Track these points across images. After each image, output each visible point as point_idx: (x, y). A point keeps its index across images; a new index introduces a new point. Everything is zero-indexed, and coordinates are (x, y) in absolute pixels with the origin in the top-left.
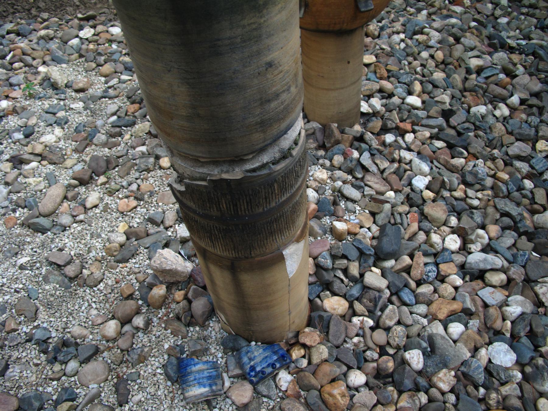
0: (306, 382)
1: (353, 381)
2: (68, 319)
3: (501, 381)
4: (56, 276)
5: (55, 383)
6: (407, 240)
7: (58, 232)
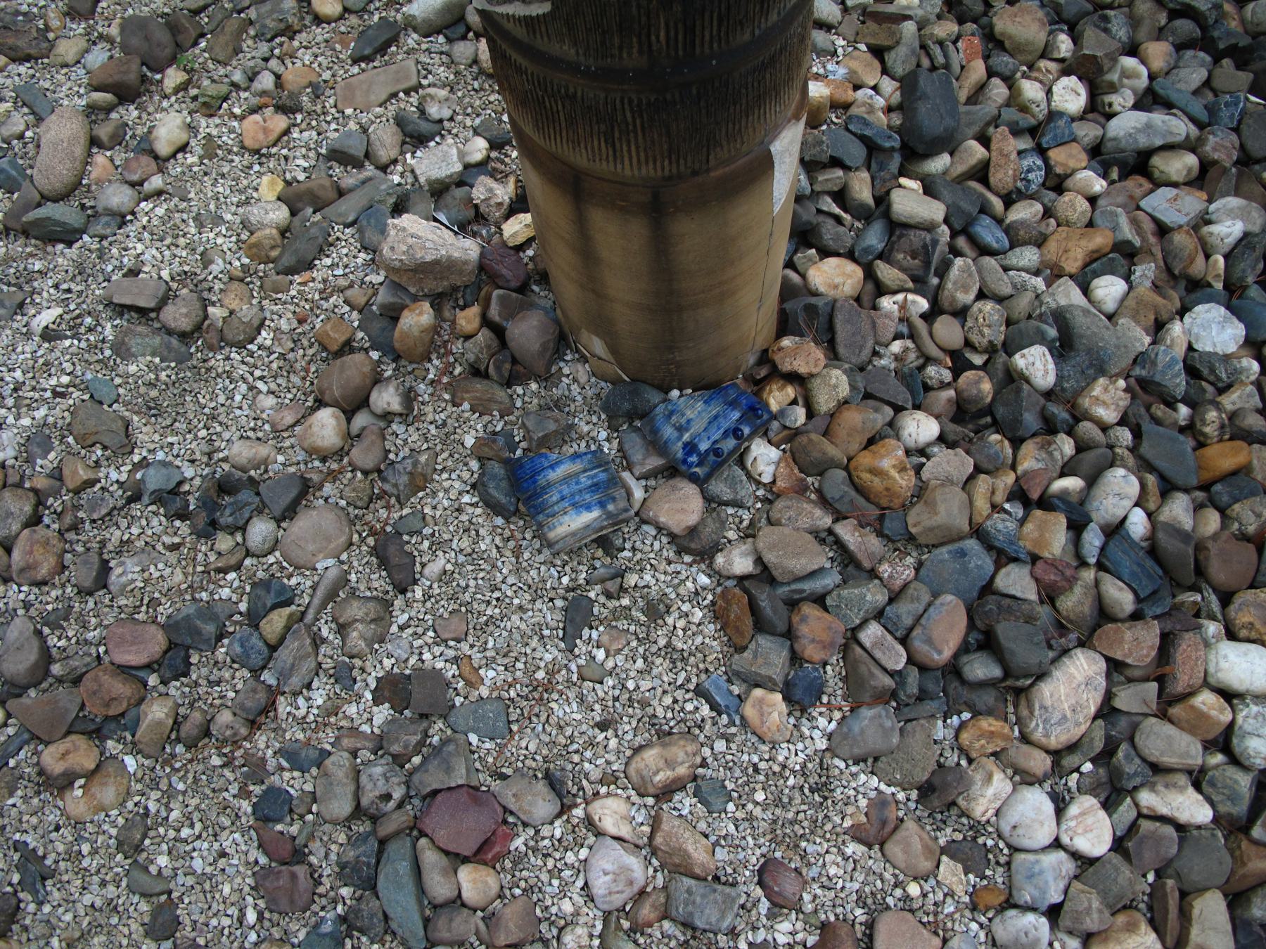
0: (815, 454)
1: (914, 435)
2: (211, 431)
3: (1220, 385)
4: (143, 338)
5: (232, 576)
6: (966, 104)
7: (108, 231)
